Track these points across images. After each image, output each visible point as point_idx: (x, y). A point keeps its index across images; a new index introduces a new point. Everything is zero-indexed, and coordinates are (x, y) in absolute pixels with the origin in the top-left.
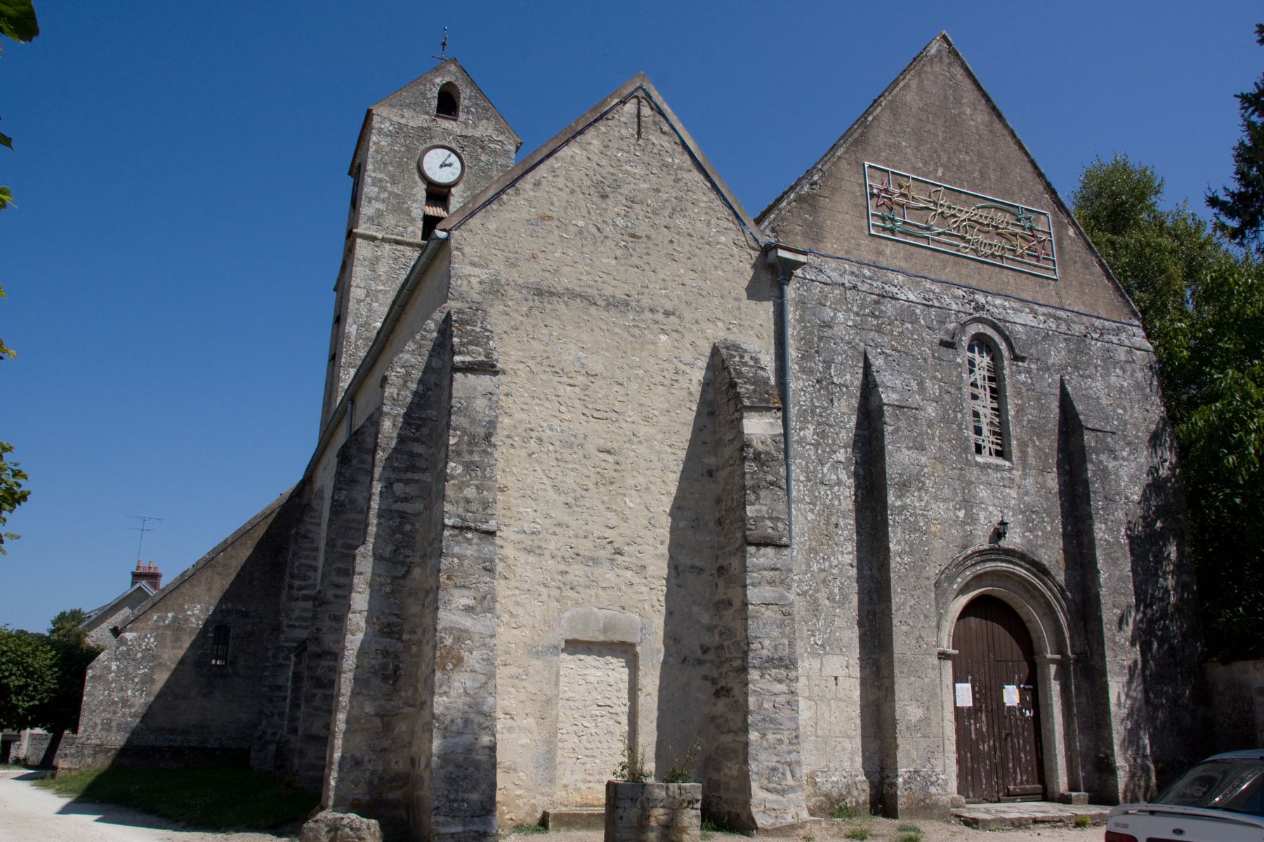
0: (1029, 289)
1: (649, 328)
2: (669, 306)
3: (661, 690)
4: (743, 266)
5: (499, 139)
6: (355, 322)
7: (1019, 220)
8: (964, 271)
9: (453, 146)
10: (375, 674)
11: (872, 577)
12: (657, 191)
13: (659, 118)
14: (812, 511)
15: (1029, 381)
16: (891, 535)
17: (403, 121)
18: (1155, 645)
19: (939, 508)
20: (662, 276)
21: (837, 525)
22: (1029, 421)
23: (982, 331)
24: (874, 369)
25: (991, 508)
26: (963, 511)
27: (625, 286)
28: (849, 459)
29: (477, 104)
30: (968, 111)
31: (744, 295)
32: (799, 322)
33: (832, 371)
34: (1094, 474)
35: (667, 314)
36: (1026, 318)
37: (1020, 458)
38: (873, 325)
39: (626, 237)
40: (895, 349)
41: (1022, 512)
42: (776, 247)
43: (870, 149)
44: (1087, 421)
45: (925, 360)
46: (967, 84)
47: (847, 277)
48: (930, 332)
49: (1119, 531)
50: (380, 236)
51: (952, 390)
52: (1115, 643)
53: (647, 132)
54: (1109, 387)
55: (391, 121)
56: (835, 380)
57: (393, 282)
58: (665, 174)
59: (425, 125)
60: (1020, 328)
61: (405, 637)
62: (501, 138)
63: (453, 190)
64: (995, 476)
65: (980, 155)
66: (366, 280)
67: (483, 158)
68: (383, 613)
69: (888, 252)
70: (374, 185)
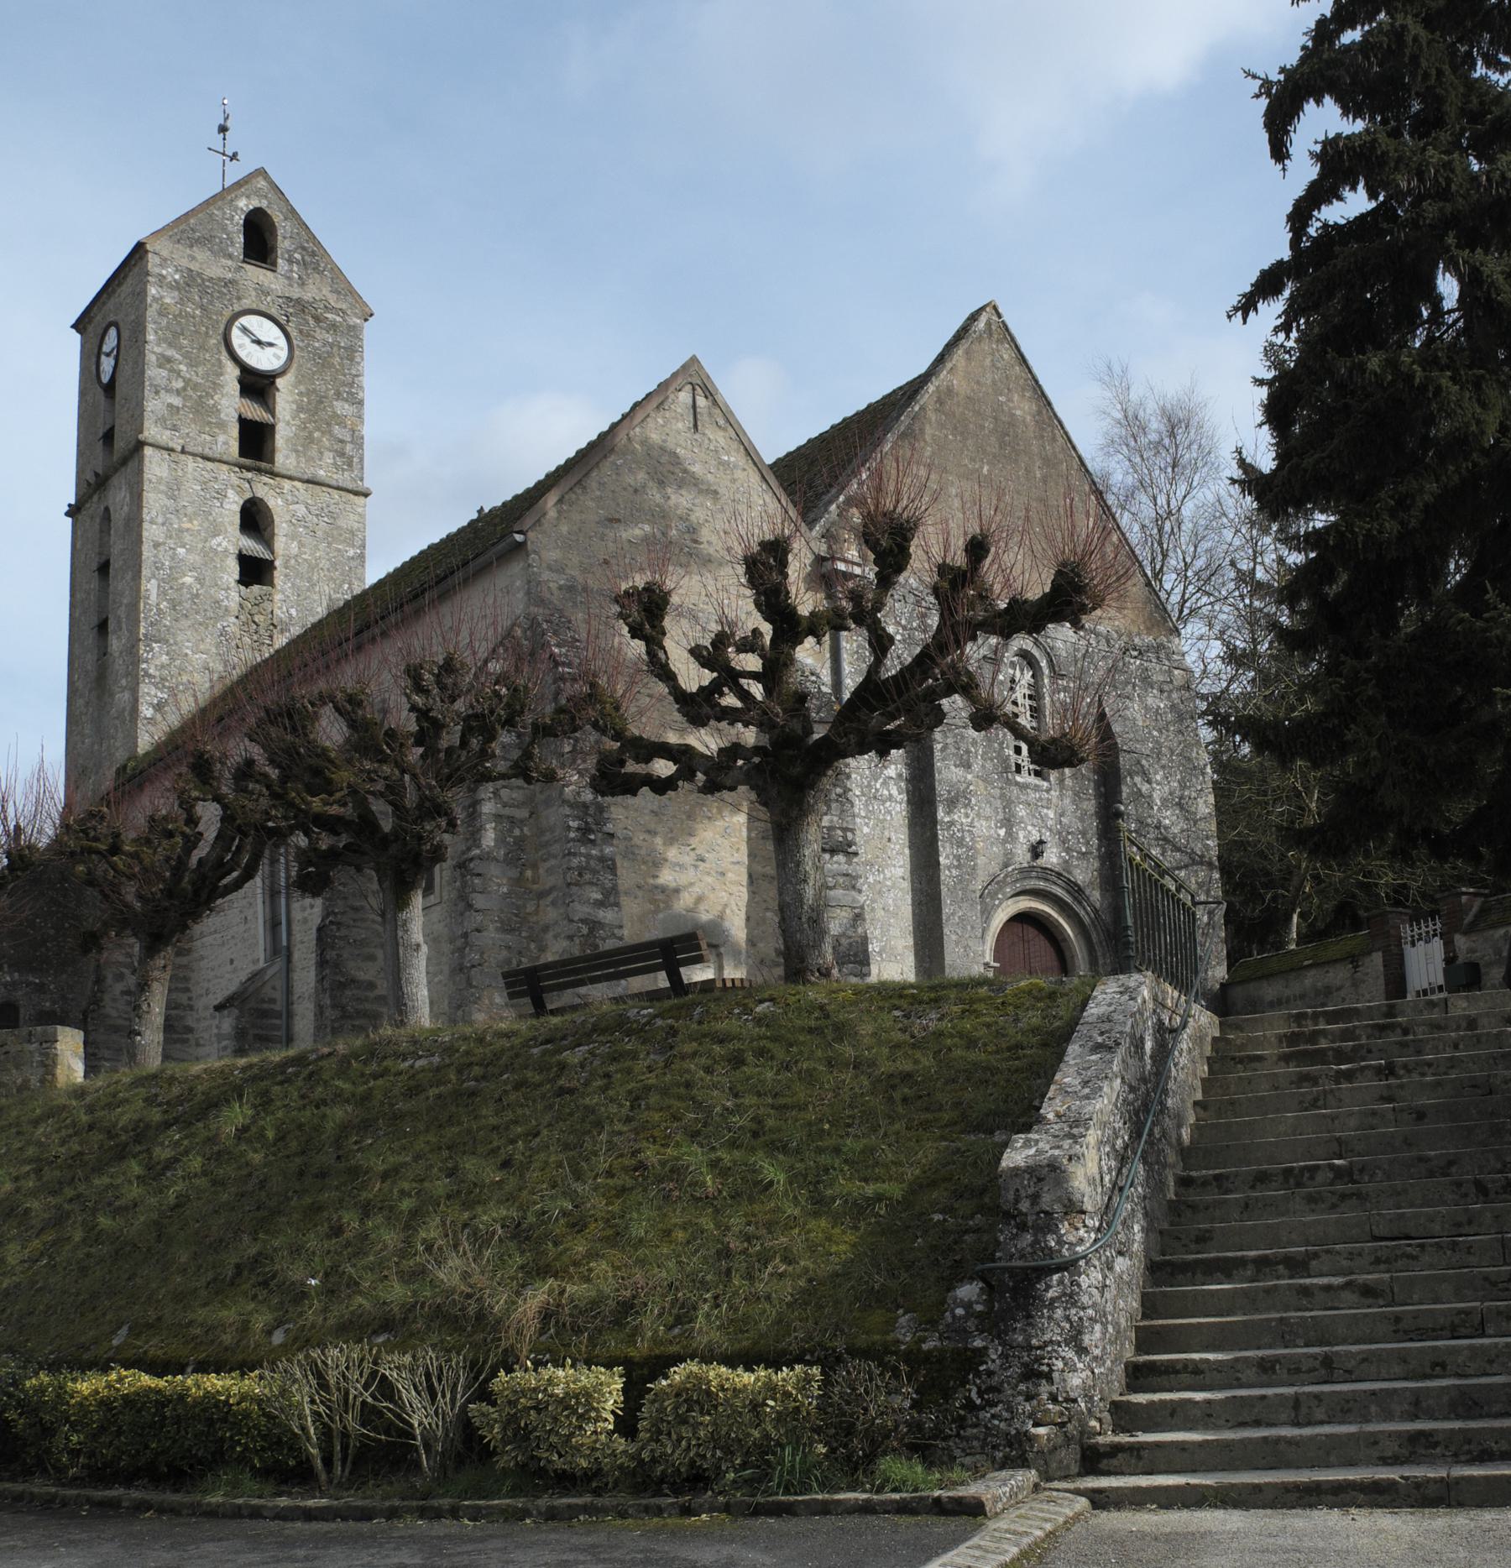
5: (338, 306)
6: (154, 576)
9: (273, 311)
14: (867, 824)
17: (194, 266)
28: (900, 775)
29: (304, 249)
63: (280, 382)
64: (1033, 796)
67: (321, 334)
68: (502, 911)
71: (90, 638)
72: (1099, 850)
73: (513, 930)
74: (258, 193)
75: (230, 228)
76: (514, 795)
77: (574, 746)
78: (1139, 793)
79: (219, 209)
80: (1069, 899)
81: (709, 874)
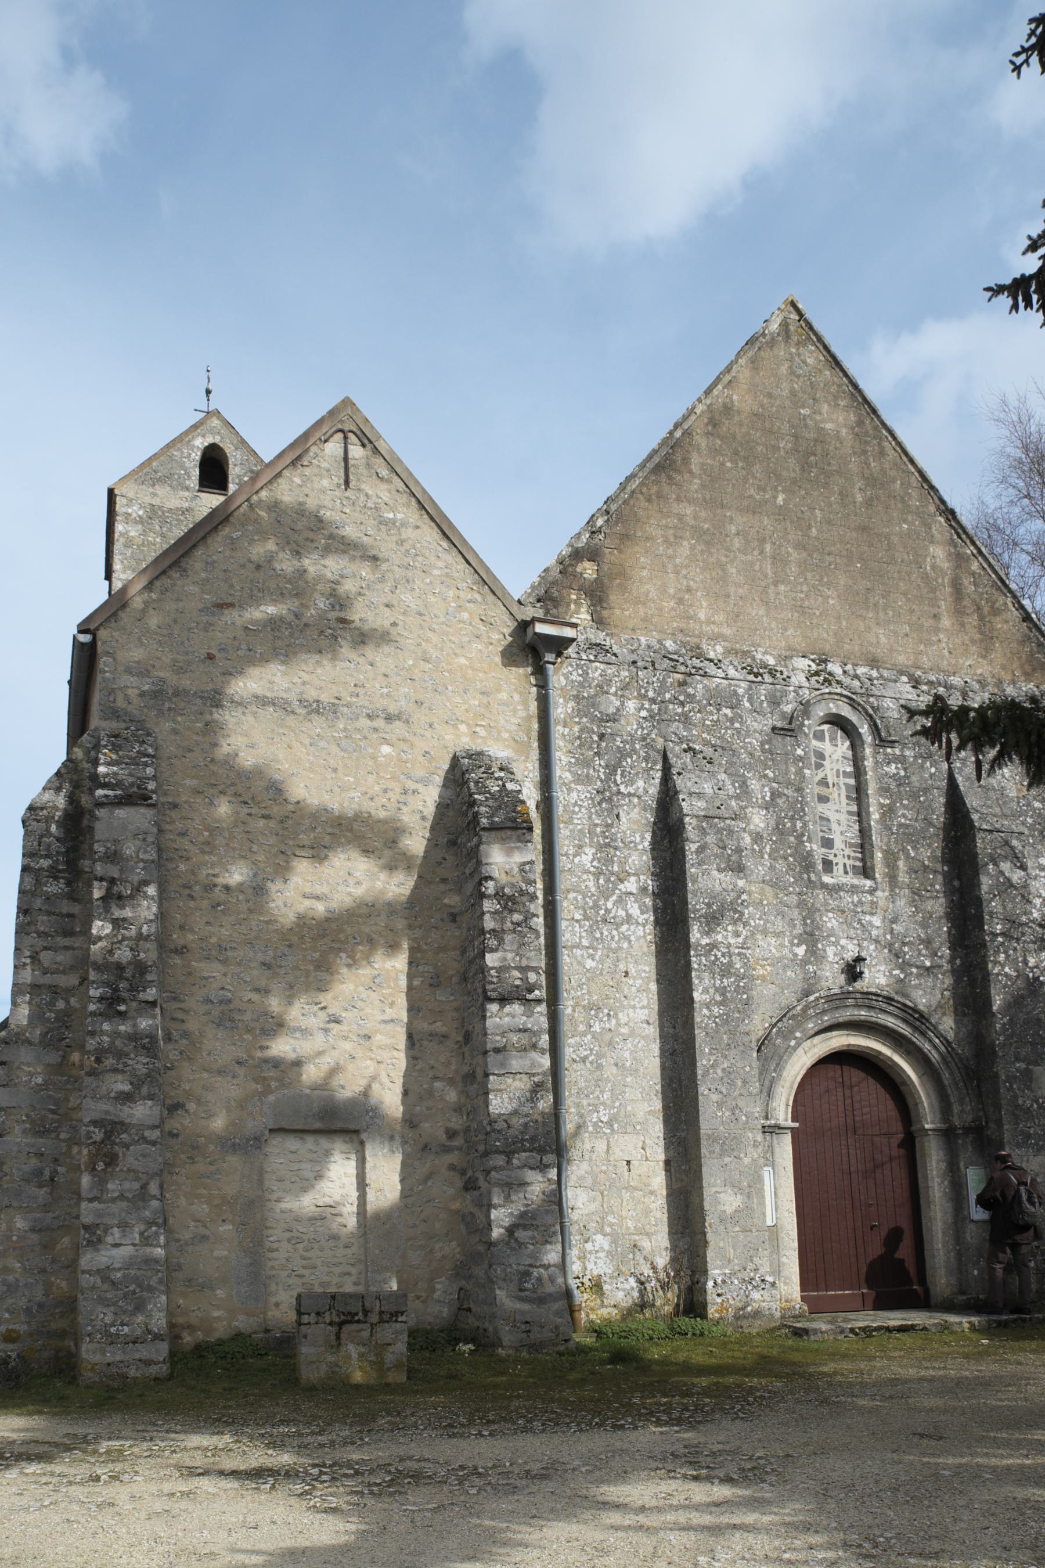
1: (365, 738)
2: (392, 709)
10: (27, 1181)
14: (592, 957)
15: (902, 773)
16: (696, 981)
17: (156, 502)
19: (769, 944)
21: (627, 974)
22: (900, 825)
23: (834, 711)
24: (674, 771)
25: (843, 942)
26: (804, 947)
27: (334, 687)
28: (644, 889)
33: (618, 777)
35: (389, 718)
37: (887, 875)
38: (676, 714)
48: (759, 718)
51: (789, 792)
53: (359, 480)
56: (622, 788)
58: (384, 535)
59: (186, 505)
64: (847, 899)
68: (34, 1108)
72: (952, 961)
73: (48, 1131)
74: (212, 431)
75: (187, 465)
76: (60, 958)
77: (109, 889)
78: (1009, 884)
79: (179, 449)
80: (905, 1030)
81: (346, 1038)
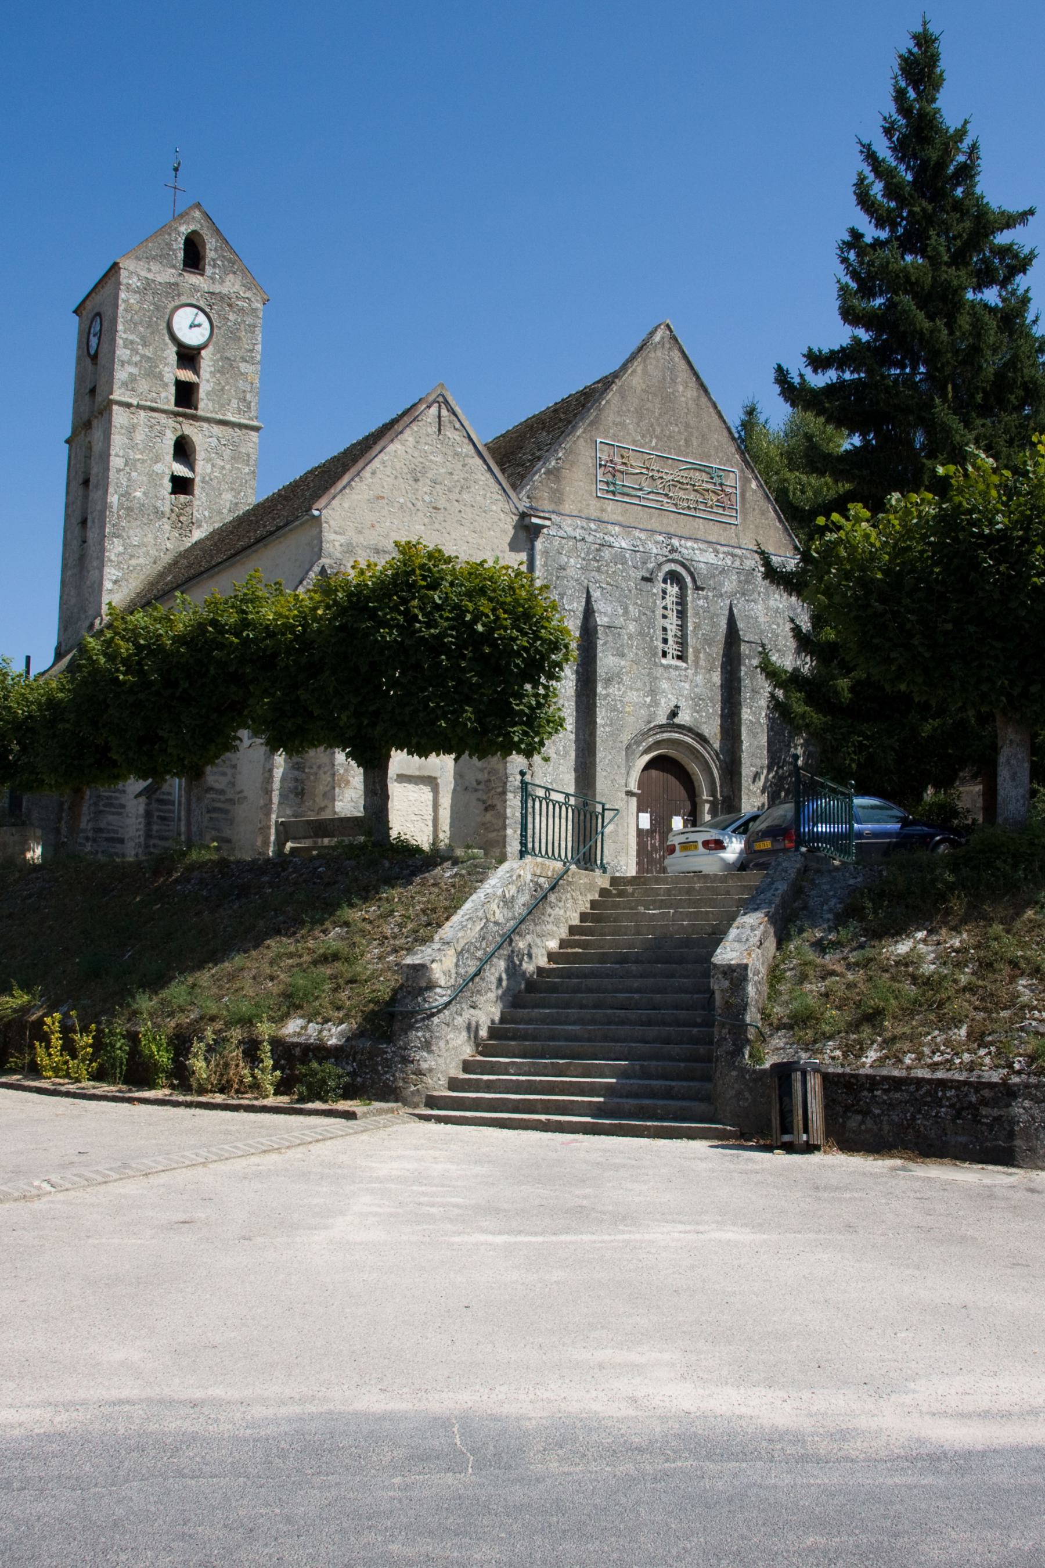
0: (715, 533)
3: (451, 807)
4: (507, 525)
5: (246, 295)
7: (712, 478)
8: (665, 521)
9: (202, 303)
10: (291, 792)
11: (584, 740)
12: (451, 474)
13: (453, 418)
17: (150, 276)
18: (783, 794)
20: (454, 537)
22: (703, 634)
24: (593, 599)
25: (670, 696)
29: (224, 257)
30: (681, 388)
31: (508, 548)
32: (543, 566)
34: (746, 674)
36: (710, 557)
39: (431, 510)
40: (608, 584)
41: (692, 699)
42: (531, 515)
43: (601, 428)
44: (745, 635)
45: (630, 591)
46: (682, 365)
47: (579, 531)
49: (760, 714)
50: (135, 403)
51: (648, 613)
52: (749, 790)
54: (768, 608)
55: (138, 275)
56: (566, 607)
57: (151, 450)
59: (173, 281)
60: (702, 565)
61: (307, 770)
62: (248, 295)
63: (203, 353)
64: (674, 673)
65: (687, 426)
66: (124, 449)
67: (232, 317)
69: (609, 509)
70: (125, 347)
71: (77, 530)
